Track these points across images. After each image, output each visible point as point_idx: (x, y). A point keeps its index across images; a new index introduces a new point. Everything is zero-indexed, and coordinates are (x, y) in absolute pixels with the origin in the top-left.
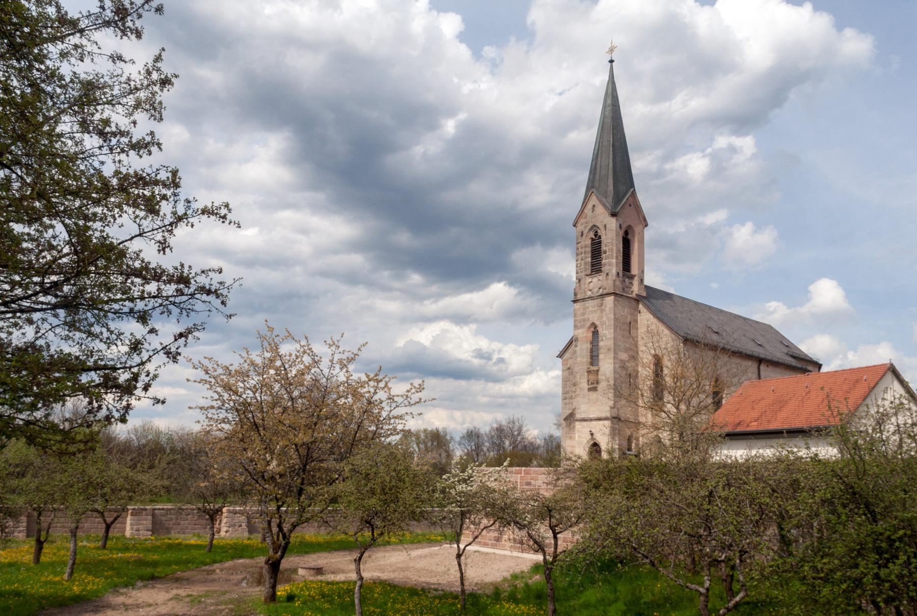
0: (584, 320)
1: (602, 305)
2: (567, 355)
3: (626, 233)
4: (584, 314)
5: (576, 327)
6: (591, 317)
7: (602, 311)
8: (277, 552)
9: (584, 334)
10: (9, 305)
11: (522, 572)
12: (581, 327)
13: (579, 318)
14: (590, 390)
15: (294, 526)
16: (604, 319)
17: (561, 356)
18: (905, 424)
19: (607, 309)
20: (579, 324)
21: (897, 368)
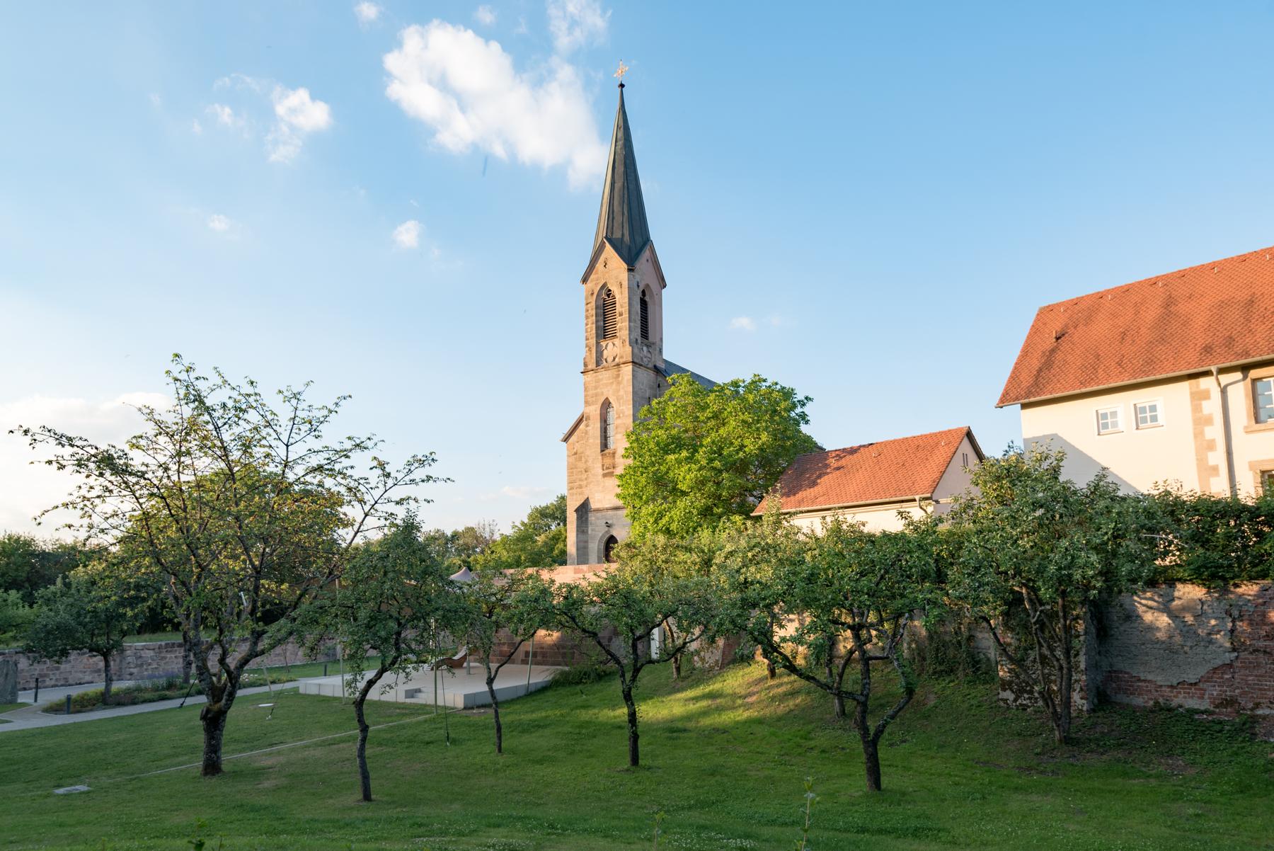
0: (596, 395)
1: (618, 376)
2: (573, 438)
3: (643, 293)
4: (596, 388)
5: (586, 403)
6: (605, 391)
7: (619, 383)
8: (219, 700)
9: (594, 411)
10: (1253, 540)
11: (874, 535)
12: (593, 403)
13: (590, 393)
14: (605, 475)
15: (245, 661)
16: (622, 393)
17: (566, 440)
18: (352, 633)
19: (625, 382)
20: (590, 400)
21: (974, 433)
